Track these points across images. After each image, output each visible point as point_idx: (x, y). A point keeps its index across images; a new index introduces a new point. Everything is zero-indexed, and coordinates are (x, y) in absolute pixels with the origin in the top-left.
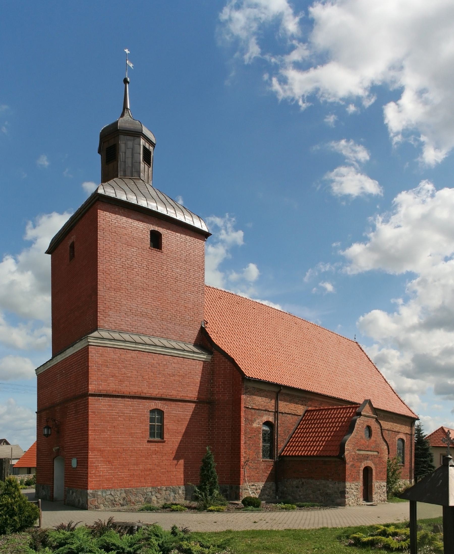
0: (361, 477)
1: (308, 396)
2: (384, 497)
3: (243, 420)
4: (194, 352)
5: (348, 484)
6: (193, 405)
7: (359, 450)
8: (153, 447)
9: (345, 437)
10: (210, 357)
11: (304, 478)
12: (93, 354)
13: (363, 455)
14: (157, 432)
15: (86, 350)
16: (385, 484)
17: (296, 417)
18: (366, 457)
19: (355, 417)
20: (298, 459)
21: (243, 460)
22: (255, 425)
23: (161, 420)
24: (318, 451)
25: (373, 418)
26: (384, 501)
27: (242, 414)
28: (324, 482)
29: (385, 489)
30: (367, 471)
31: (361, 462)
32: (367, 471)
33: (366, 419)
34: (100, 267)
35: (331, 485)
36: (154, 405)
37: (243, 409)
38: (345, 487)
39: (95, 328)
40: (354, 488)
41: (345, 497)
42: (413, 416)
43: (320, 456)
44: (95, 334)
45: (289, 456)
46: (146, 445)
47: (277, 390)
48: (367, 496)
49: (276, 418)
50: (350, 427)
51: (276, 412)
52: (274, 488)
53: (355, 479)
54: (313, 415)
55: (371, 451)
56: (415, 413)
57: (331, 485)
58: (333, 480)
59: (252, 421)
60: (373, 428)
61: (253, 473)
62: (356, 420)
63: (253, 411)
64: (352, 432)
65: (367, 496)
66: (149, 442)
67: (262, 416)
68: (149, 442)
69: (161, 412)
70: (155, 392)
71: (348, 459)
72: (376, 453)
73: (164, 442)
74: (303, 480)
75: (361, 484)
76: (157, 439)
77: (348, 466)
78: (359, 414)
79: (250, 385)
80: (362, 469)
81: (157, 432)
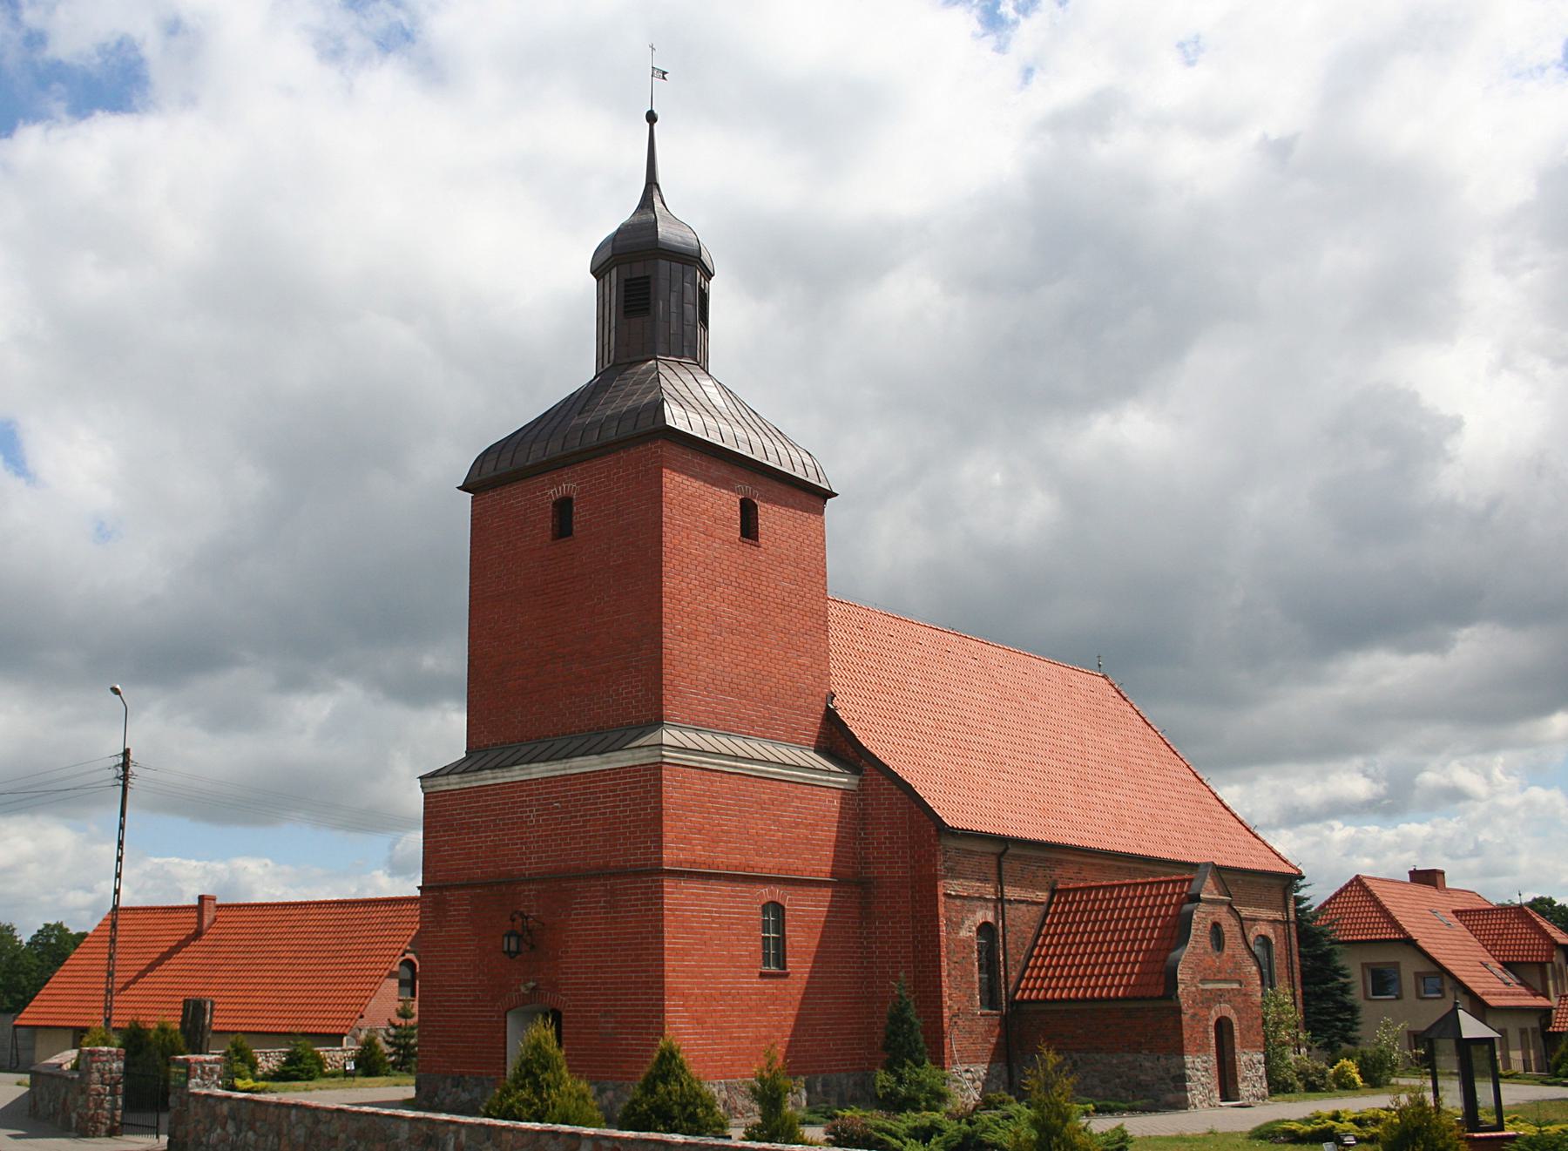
0: (1213, 1042)
1: (1054, 856)
2: (1262, 1088)
3: (942, 921)
4: (829, 772)
5: (1188, 1059)
6: (827, 893)
7: (1203, 981)
8: (770, 986)
9: (1173, 955)
10: (855, 780)
11: (1077, 1051)
12: (673, 792)
13: (1211, 991)
14: (776, 953)
15: (655, 771)
16: (1261, 1057)
17: (1035, 908)
18: (1219, 996)
19: (1187, 907)
20: (1075, 1006)
21: (946, 1013)
22: (963, 934)
23: (780, 926)
24: (1126, 987)
25: (1222, 902)
26: (1263, 1098)
27: (942, 910)
28: (1129, 1057)
29: (1262, 1070)
30: (1223, 1026)
31: (1209, 1008)
32: (1223, 1026)
33: (1209, 908)
34: (668, 585)
35: (1147, 1064)
36: (766, 893)
37: (942, 898)
38: (1183, 1066)
39: (657, 722)
40: (1200, 1067)
41: (1185, 1089)
42: (1286, 869)
43: (1135, 999)
44: (669, 736)
45: (1037, 1001)
46: (757, 983)
47: (998, 849)
48: (1228, 1089)
49: (1001, 914)
50: (1179, 930)
51: (1001, 900)
52: (1005, 1076)
53: (1202, 1048)
54: (1074, 900)
55: (1225, 981)
56: (1291, 861)
57: (1147, 1064)
58: (1151, 1051)
59: (959, 925)
60: (1225, 928)
61: (966, 1044)
62: (1191, 913)
63: (958, 902)
64: (1186, 942)
65: (1228, 1089)
66: (762, 975)
67: (974, 912)
68: (762, 975)
69: (776, 909)
70: (767, 864)
71: (1185, 1002)
72: (1236, 986)
73: (786, 975)
74: (1076, 1056)
75: (1213, 1058)
76: (773, 969)
77: (1185, 1018)
78: (1195, 899)
79: (952, 843)
80: (1212, 1023)
81: (776, 953)
